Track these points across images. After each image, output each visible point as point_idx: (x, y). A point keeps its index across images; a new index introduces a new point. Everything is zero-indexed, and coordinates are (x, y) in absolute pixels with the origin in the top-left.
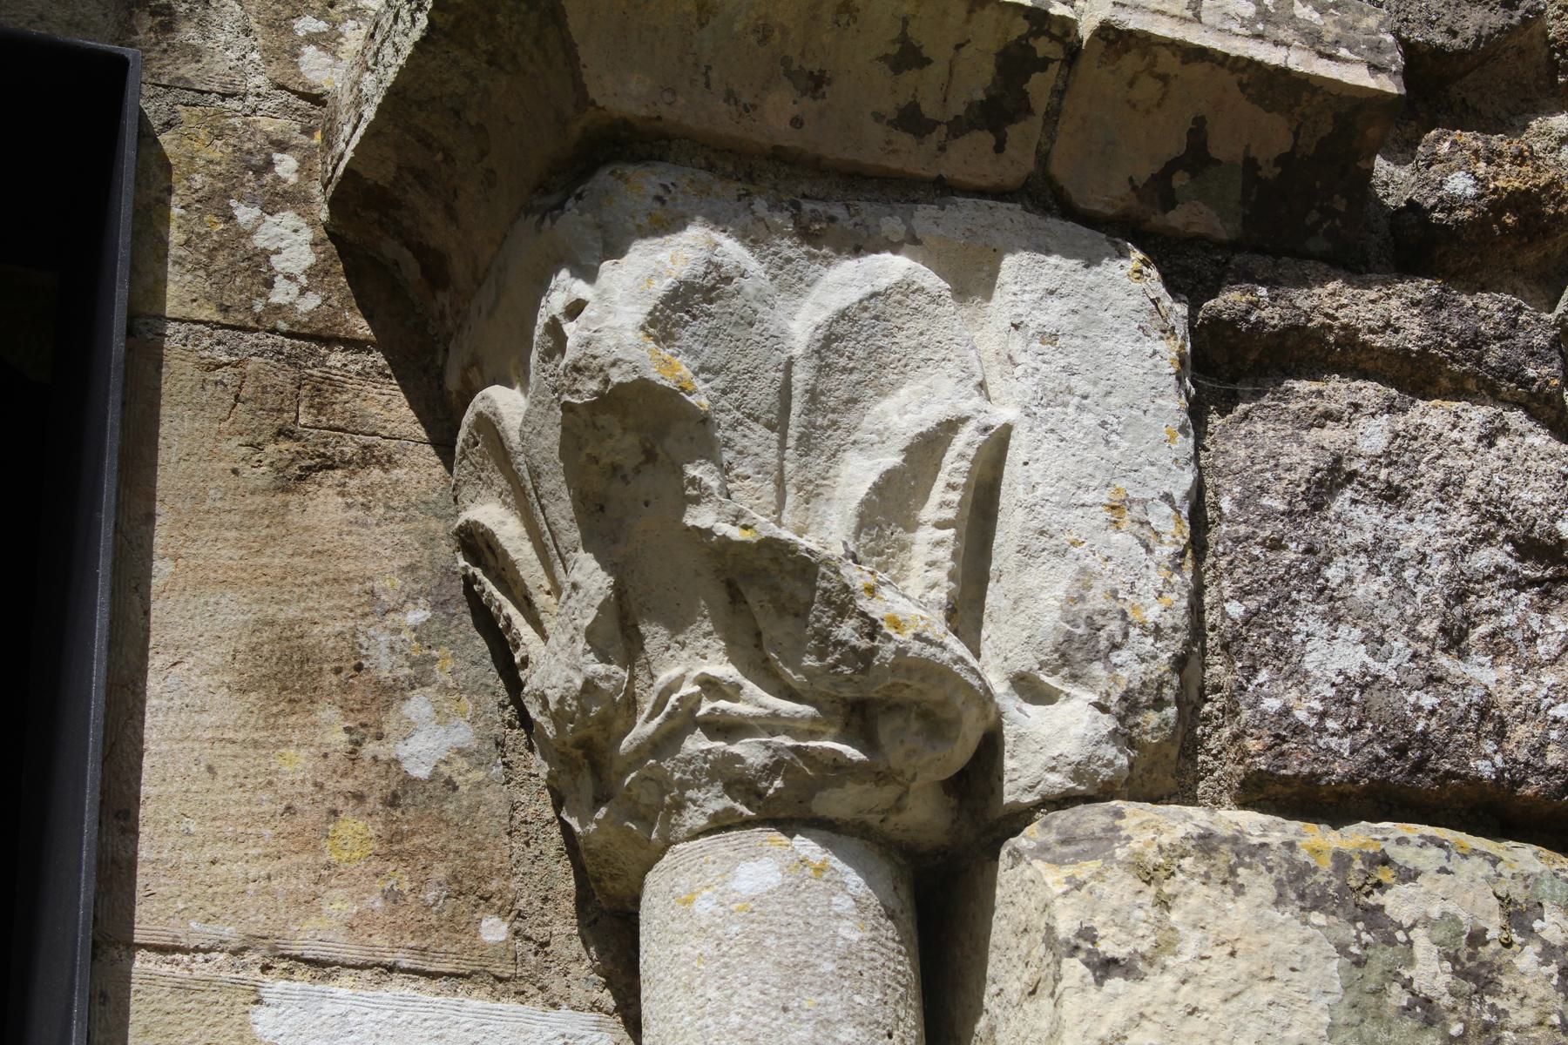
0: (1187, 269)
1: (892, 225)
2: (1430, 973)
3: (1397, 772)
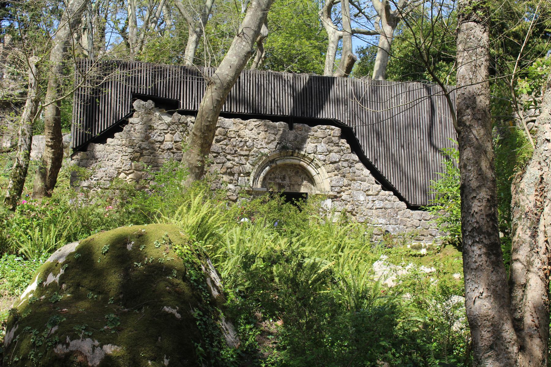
0: (332, 199)
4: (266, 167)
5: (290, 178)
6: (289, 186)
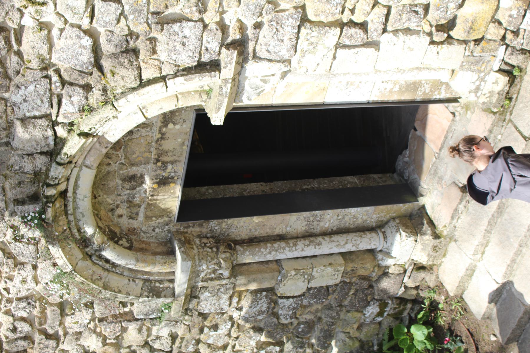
0: (245, 60)
1: (243, 85)
2: (311, 47)
3: (294, 48)
4: (107, 261)
5: (132, 165)
6: (165, 165)
